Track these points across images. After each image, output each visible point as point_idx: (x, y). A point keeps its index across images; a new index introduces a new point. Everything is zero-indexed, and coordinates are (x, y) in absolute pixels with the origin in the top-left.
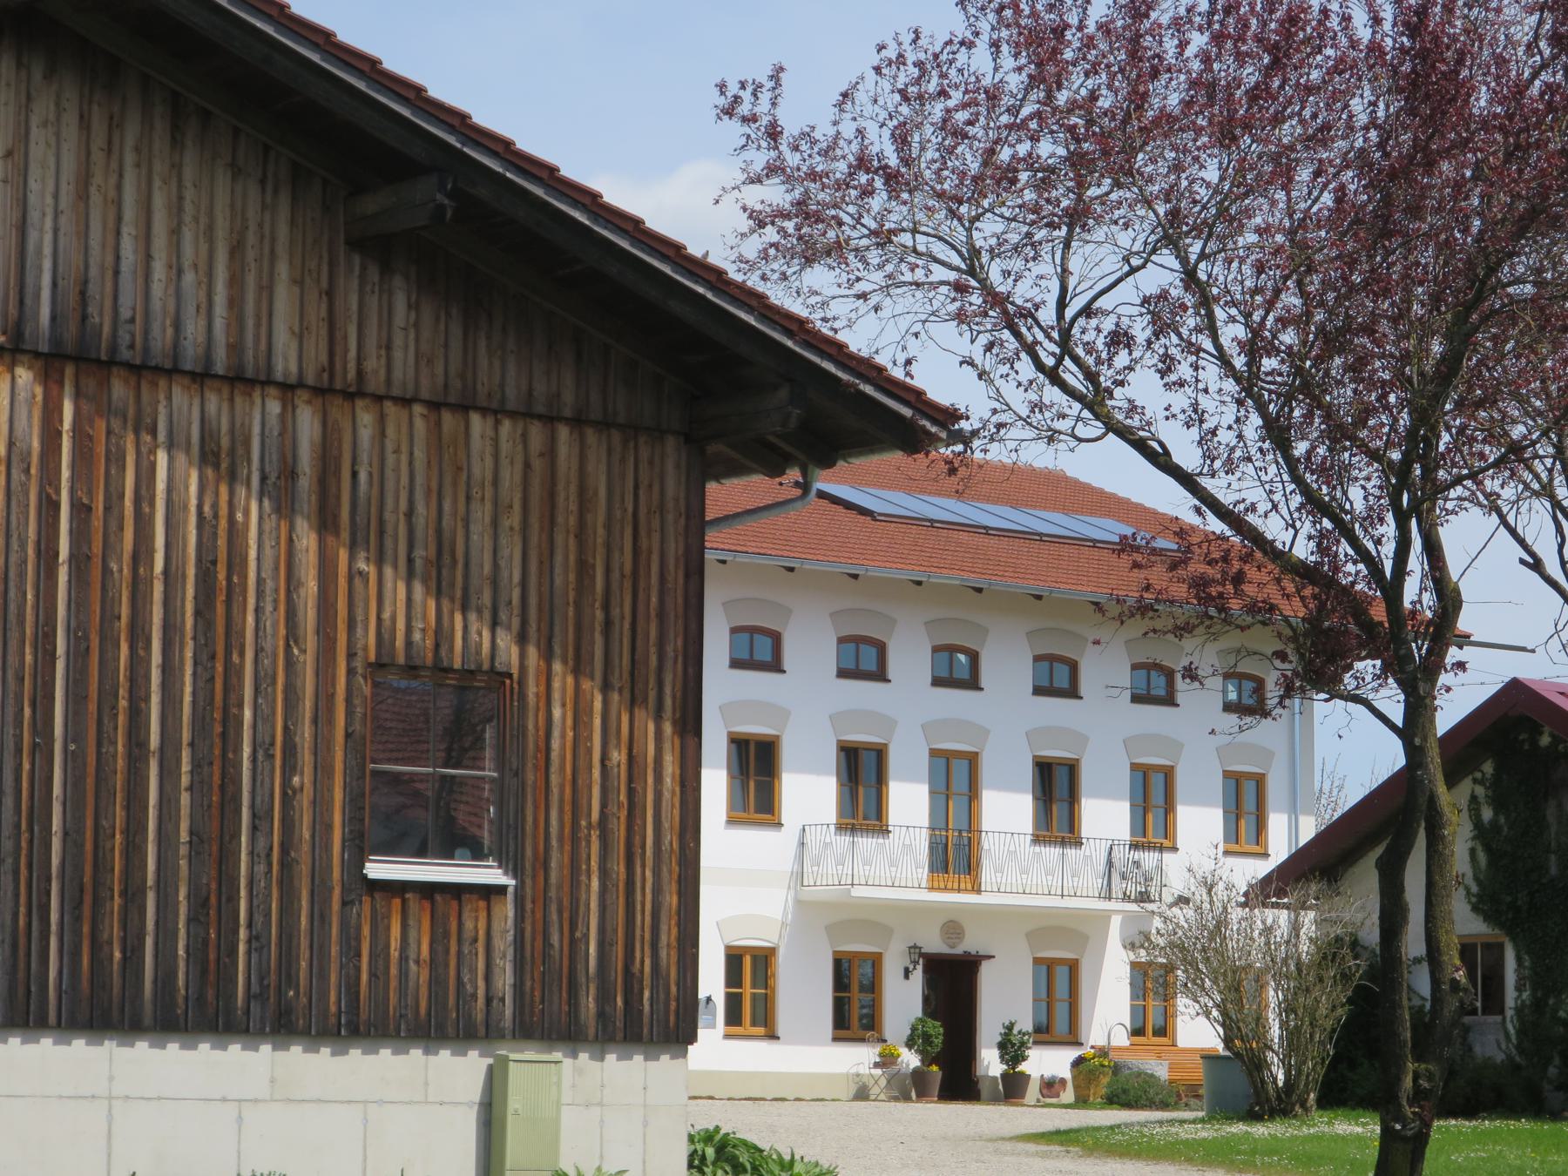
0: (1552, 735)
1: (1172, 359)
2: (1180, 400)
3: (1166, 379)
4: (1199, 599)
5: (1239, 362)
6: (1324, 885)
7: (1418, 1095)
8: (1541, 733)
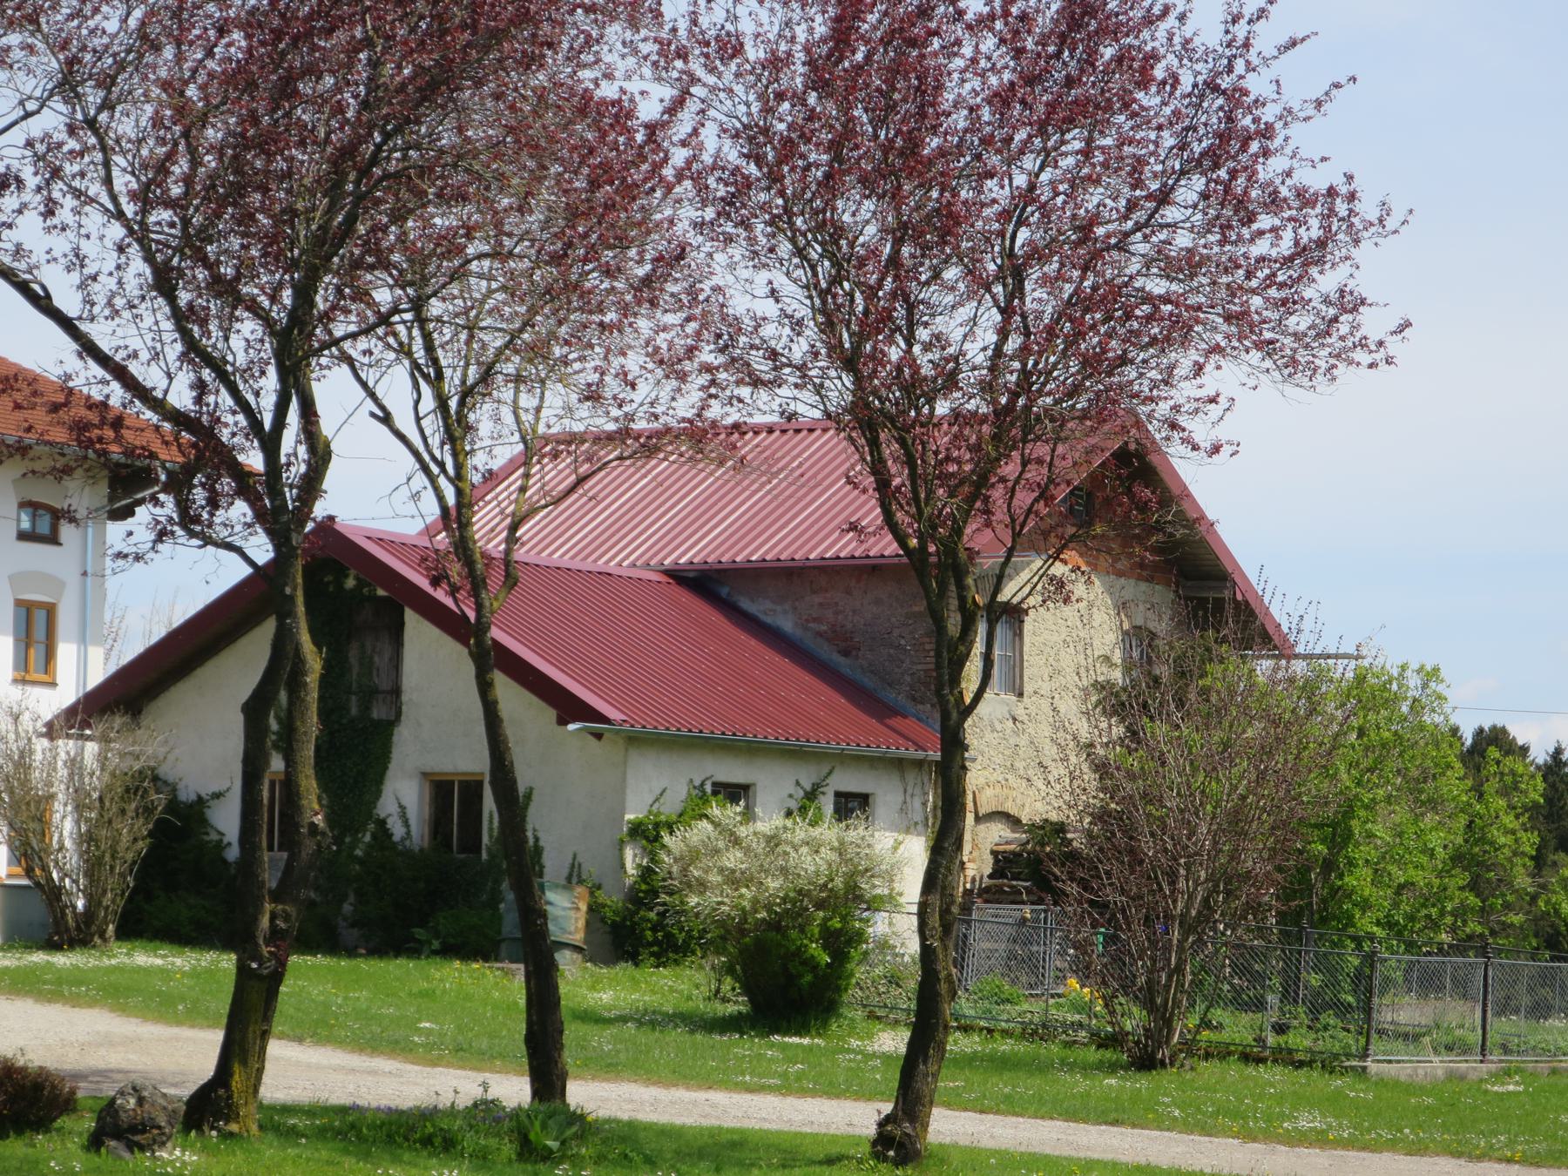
0: (357, 578)
1: (56, 203)
2: (62, 244)
3: (49, 222)
4: (80, 442)
5: (129, 209)
6: (126, 719)
7: (275, 935)
8: (347, 576)
